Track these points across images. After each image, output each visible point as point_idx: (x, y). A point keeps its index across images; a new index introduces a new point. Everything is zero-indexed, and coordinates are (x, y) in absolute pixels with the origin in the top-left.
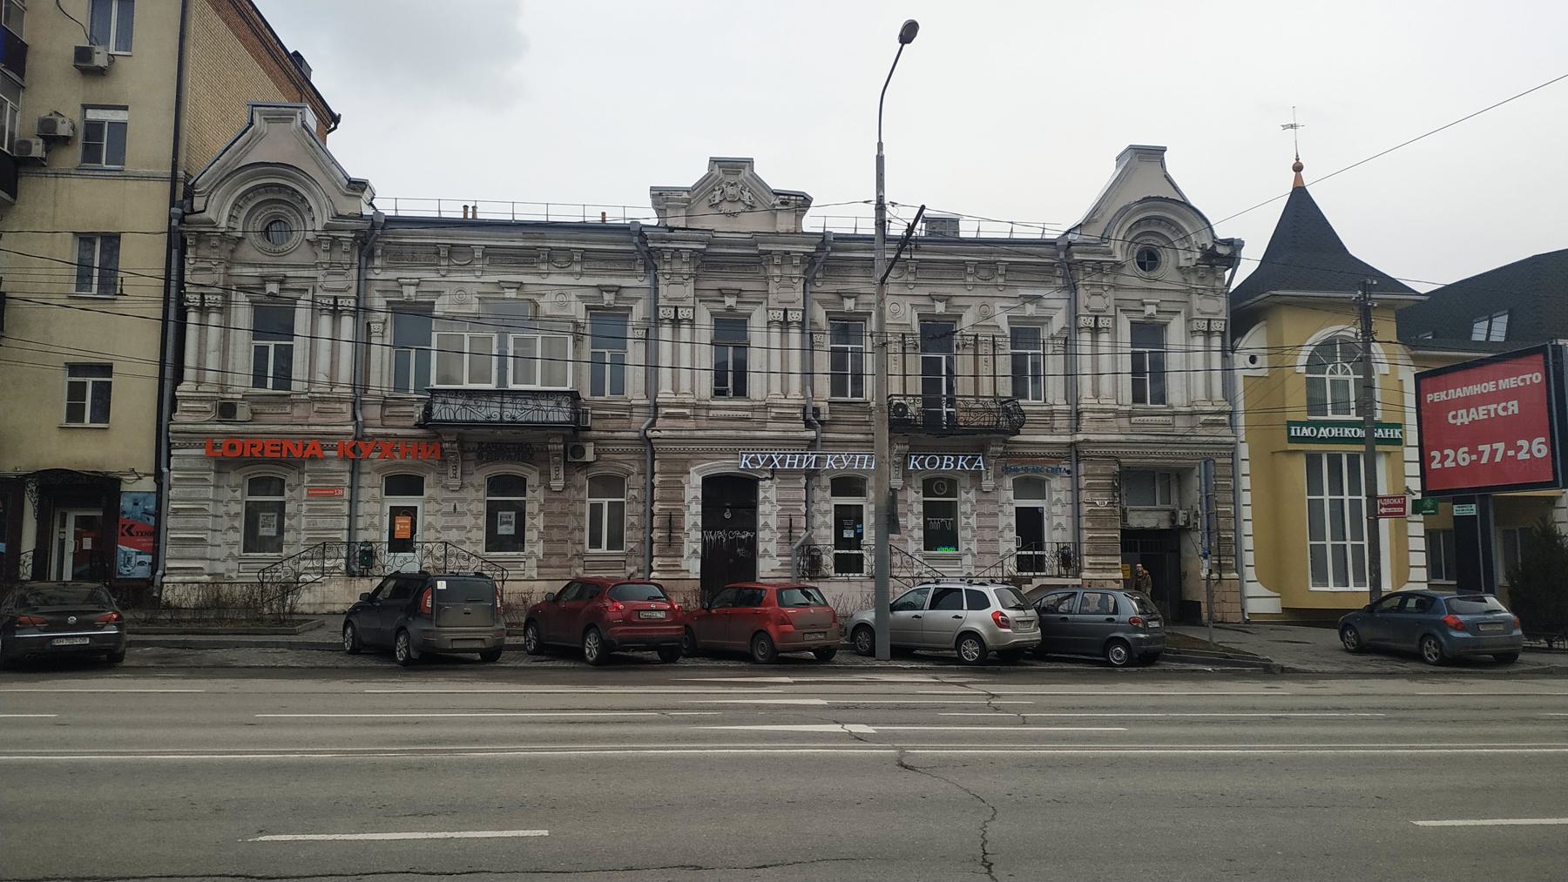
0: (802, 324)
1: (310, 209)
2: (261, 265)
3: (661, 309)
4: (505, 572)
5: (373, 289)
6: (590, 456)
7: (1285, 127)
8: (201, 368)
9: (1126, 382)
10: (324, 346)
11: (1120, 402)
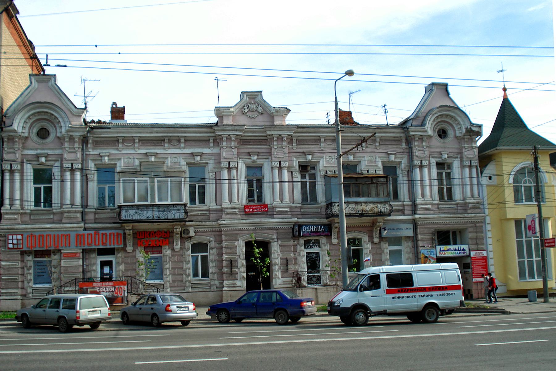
0: (82, 169)
1: (59, 122)
2: (36, 149)
3: (273, 162)
4: (159, 290)
5: (89, 158)
6: (192, 234)
7: (499, 72)
8: (12, 199)
9: (244, 188)
10: (68, 184)
11: (433, 199)
